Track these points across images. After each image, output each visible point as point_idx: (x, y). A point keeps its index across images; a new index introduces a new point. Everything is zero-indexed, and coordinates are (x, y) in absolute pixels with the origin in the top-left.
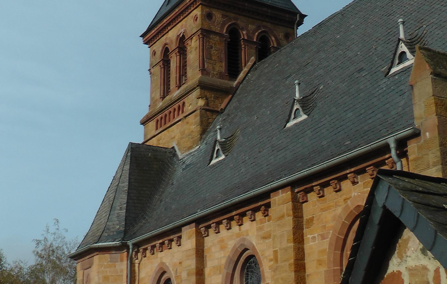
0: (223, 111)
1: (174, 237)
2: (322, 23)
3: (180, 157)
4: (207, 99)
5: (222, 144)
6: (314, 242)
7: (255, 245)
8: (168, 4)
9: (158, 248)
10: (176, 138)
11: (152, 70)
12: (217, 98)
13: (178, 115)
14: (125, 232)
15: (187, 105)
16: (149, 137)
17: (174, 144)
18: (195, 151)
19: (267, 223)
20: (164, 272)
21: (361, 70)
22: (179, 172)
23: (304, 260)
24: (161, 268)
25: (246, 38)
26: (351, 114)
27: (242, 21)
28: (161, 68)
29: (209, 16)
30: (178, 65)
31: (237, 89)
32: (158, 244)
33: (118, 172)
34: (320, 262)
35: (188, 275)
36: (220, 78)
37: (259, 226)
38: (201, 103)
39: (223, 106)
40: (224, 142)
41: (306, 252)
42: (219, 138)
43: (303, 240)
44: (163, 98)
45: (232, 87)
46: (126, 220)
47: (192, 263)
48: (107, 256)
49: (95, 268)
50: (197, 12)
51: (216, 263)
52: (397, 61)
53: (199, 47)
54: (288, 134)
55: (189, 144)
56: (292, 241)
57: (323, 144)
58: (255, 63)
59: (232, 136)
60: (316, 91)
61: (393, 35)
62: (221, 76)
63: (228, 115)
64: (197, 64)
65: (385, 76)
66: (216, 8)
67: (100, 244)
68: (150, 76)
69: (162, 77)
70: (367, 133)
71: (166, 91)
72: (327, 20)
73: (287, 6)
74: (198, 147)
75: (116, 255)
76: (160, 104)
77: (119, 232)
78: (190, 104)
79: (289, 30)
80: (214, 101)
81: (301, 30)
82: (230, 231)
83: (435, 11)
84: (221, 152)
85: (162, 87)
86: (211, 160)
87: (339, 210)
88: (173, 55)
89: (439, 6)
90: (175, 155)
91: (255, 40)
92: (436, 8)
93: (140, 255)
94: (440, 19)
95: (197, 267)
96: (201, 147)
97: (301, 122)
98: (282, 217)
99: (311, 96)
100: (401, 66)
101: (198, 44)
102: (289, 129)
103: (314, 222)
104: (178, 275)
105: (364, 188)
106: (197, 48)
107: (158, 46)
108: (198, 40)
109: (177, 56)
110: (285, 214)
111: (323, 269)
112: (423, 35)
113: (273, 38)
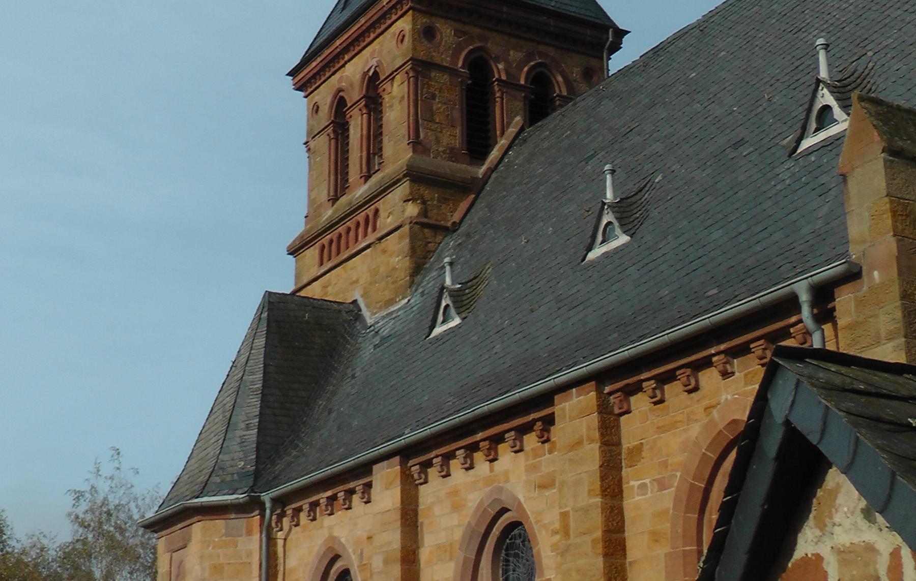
0: (456, 226)
1: (357, 484)
2: (660, 47)
3: (369, 321)
4: (424, 202)
5: (454, 295)
7: (522, 501)
8: (343, 9)
9: (324, 508)
10: (361, 282)
11: (312, 144)
12: (444, 200)
13: (365, 234)
14: (257, 475)
15: (382, 214)
16: (305, 280)
17: (357, 296)
18: (399, 309)
19: (547, 456)
20: (336, 557)
22: (367, 351)
23: (624, 531)
24: (330, 549)
25: (504, 77)
27: (494, 44)
28: (330, 140)
29: (428, 33)
30: (365, 132)
31: (486, 182)
32: (325, 500)
33: (242, 351)
34: (655, 537)
35: (386, 562)
36: (450, 159)
38: (412, 210)
39: (456, 217)
40: (459, 290)
41: (628, 514)
42: (448, 281)
43: (621, 491)
44: (334, 200)
45: (474, 179)
46: (258, 449)
47: (393, 539)
48: (219, 524)
49: (194, 547)
50: (404, 25)
51: (442, 537)
52: (813, 125)
55: (387, 295)
56: (598, 492)
57: (661, 294)
58: (522, 130)
60: (648, 185)
61: (805, 72)
62: (453, 154)
63: (468, 235)
64: (403, 130)
65: (790, 156)
67: (205, 499)
69: (333, 158)
70: (752, 272)
71: (340, 186)
72: (669, 40)
73: (588, 13)
74: (406, 300)
75: (239, 522)
76: (328, 213)
77: (243, 475)
78: (390, 213)
79: (593, 62)
80: (439, 208)
81: (617, 62)
82: (471, 472)
83: (892, 24)
84: (452, 311)
85: (332, 177)
86: (432, 327)
87: (695, 430)
88: (355, 112)
90: (358, 317)
91: (522, 82)
92: (893, 16)
93: (286, 521)
95: (403, 547)
96: (412, 301)
97: (617, 250)
98: (579, 443)
99: (638, 197)
100: (822, 135)
101: (406, 90)
103: (644, 454)
104: (364, 562)
105: (746, 384)
106: (403, 98)
107: (324, 95)
109: (362, 115)
111: (662, 550)
112: (866, 72)
113: (560, 79)
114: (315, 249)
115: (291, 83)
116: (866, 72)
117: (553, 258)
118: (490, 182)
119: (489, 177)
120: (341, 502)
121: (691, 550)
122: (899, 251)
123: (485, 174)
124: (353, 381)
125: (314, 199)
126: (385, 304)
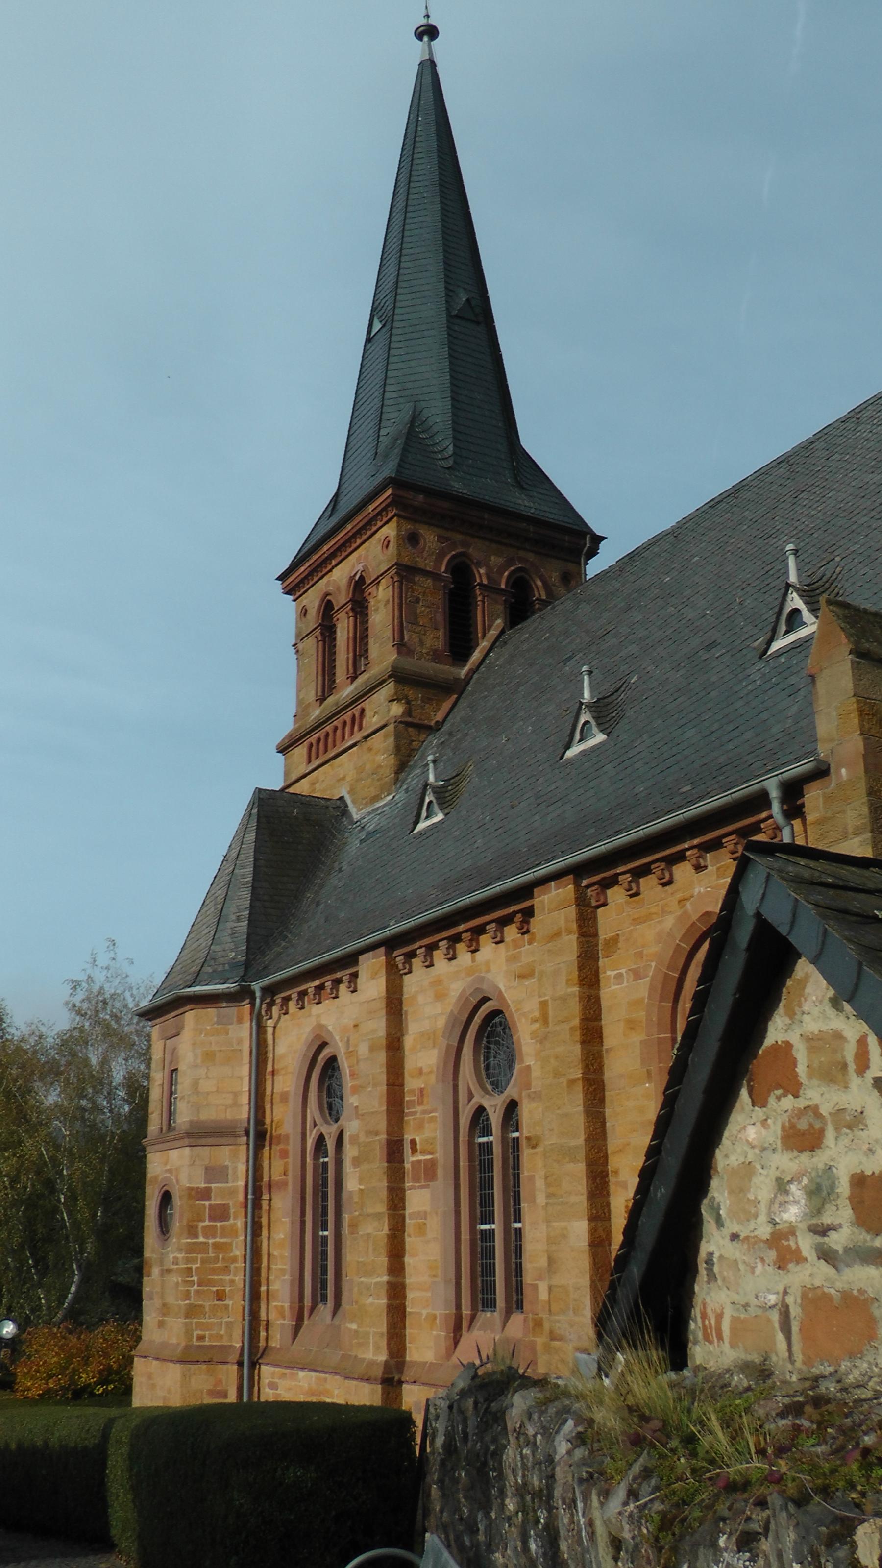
0: (439, 725)
3: (356, 816)
4: (408, 702)
5: (438, 791)
6: (619, 984)
7: (503, 990)
8: (331, 516)
9: (312, 997)
10: (348, 779)
11: (300, 646)
12: (427, 700)
13: (352, 733)
14: (247, 965)
16: (294, 777)
17: (344, 792)
19: (527, 947)
20: (324, 1045)
21: (712, 645)
22: (353, 846)
25: (485, 582)
27: (476, 550)
28: (318, 642)
29: (412, 539)
30: (351, 635)
31: (468, 683)
32: (313, 989)
33: (233, 846)
35: (372, 1049)
36: (433, 661)
37: (510, 953)
38: (397, 709)
39: (439, 717)
40: (442, 786)
41: (605, 1003)
42: (431, 778)
44: (322, 700)
45: (457, 680)
46: (248, 941)
47: (378, 1026)
48: (211, 1012)
49: (187, 1035)
50: (389, 531)
52: (783, 628)
53: (393, 601)
54: (568, 771)
55: (373, 792)
57: (637, 790)
58: (502, 632)
60: (625, 686)
62: (436, 656)
63: (451, 734)
64: (389, 633)
65: (760, 657)
69: (320, 659)
70: (724, 769)
71: (328, 686)
74: (391, 797)
75: (230, 1011)
76: (316, 713)
77: (234, 965)
79: (571, 567)
80: (422, 707)
81: (594, 567)
84: (436, 807)
85: (320, 678)
86: (416, 823)
87: (669, 922)
88: (342, 615)
90: (345, 812)
91: (503, 586)
92: (860, 522)
93: (275, 1010)
97: (594, 748)
98: (558, 934)
99: (614, 697)
100: (792, 638)
101: (391, 593)
102: (571, 761)
103: (620, 945)
104: (351, 1049)
105: (719, 877)
106: (388, 601)
107: (312, 598)
111: (637, 1038)
112: (834, 576)
113: (539, 583)
114: (386, 736)
115: (281, 587)
122: (865, 749)
123: (467, 675)
124: (340, 875)
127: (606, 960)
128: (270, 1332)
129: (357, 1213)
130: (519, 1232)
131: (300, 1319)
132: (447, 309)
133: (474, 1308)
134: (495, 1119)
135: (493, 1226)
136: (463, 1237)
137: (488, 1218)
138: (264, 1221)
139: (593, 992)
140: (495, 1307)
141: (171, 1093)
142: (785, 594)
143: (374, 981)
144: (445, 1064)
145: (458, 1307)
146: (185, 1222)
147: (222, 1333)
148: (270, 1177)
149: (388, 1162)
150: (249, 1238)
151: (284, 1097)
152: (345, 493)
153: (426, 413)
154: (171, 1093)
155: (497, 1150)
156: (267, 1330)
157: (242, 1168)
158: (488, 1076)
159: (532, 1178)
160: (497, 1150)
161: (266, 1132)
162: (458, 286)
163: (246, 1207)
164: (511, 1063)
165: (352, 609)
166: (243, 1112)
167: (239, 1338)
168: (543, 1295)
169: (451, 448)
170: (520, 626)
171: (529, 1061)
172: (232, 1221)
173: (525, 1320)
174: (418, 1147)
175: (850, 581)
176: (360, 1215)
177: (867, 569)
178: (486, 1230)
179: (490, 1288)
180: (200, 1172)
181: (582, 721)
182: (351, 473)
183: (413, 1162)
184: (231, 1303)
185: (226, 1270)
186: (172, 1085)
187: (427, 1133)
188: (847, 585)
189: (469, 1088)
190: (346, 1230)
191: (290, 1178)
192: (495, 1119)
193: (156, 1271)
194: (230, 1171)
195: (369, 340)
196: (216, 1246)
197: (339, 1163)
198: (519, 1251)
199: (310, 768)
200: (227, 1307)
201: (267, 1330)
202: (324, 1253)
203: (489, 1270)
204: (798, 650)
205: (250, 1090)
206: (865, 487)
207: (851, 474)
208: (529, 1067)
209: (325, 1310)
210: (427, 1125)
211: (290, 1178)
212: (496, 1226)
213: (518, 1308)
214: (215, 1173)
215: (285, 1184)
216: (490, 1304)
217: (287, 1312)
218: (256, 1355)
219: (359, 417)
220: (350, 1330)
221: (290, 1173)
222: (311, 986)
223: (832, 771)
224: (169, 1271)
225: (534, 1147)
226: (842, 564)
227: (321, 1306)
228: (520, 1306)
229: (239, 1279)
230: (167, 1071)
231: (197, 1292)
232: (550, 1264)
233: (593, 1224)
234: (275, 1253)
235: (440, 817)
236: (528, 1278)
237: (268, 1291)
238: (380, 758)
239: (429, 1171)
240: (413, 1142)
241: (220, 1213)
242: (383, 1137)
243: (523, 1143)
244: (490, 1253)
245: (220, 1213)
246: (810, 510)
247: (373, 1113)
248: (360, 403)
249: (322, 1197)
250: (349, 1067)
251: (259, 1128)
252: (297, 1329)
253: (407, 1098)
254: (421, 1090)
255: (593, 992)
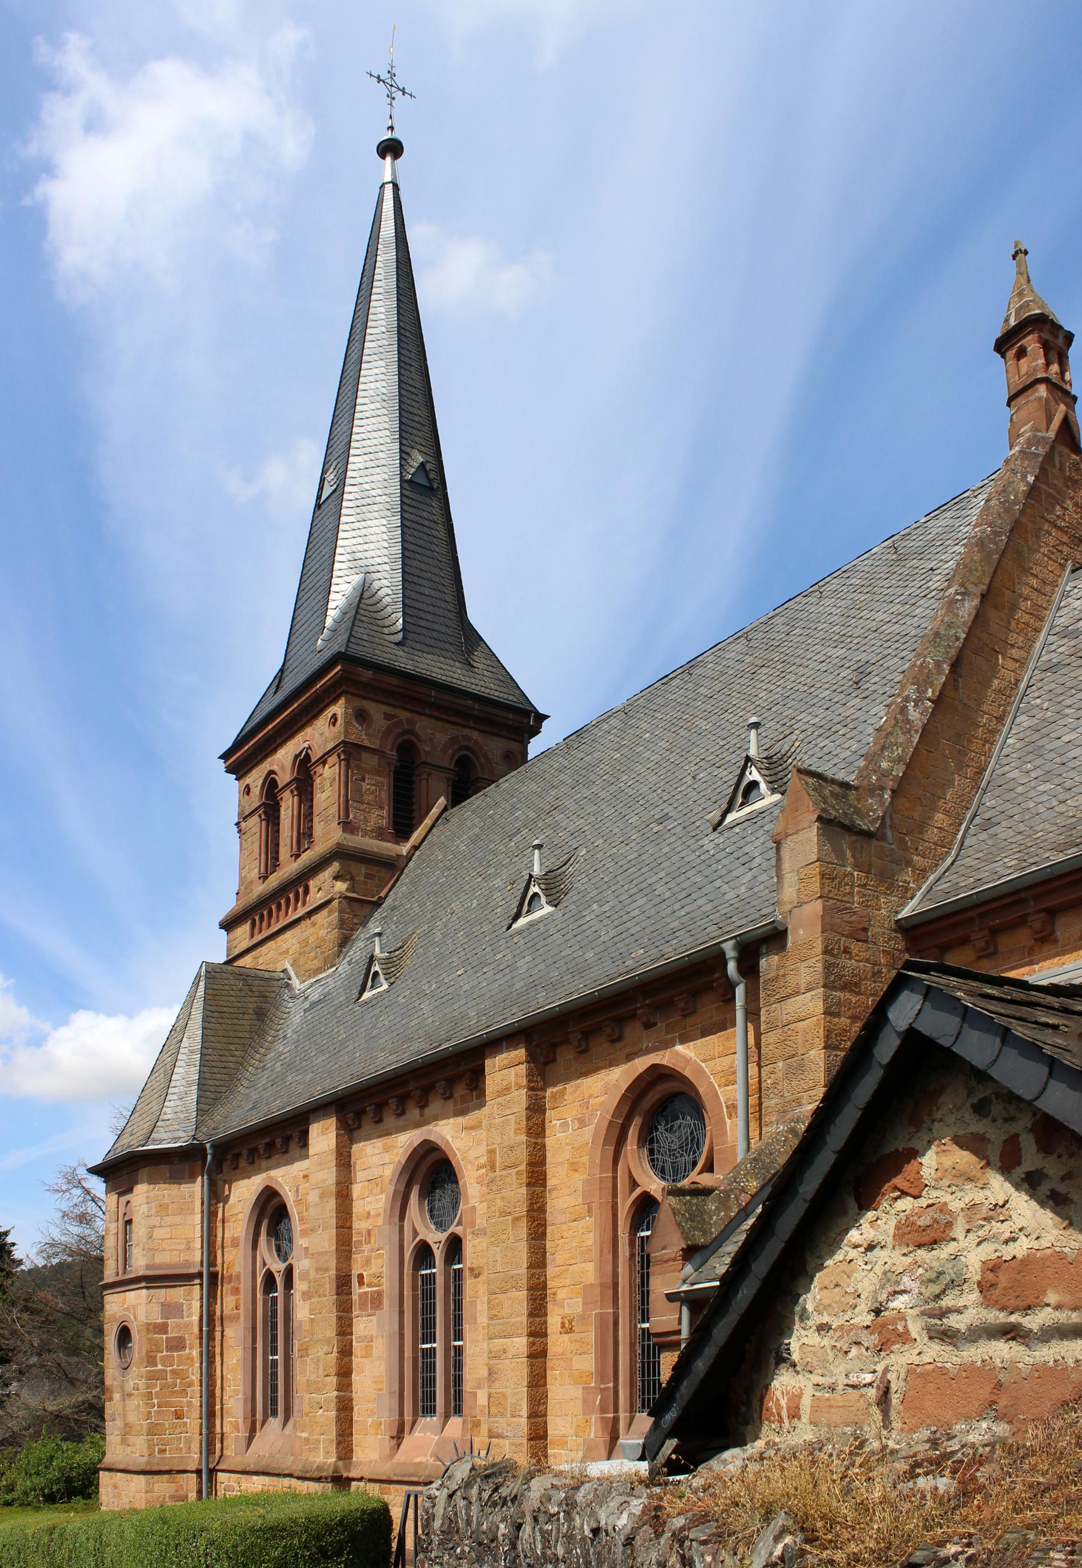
2: (584, 729)
6: (564, 1132)
7: (450, 1140)
8: (276, 692)
9: (262, 1152)
11: (243, 825)
13: (295, 909)
16: (236, 952)
18: (327, 977)
19: (475, 1101)
21: (666, 817)
23: (545, 1164)
26: (644, 900)
28: (261, 821)
29: (361, 716)
30: (295, 813)
31: (410, 860)
32: (263, 1145)
33: (181, 1016)
34: (574, 1167)
35: (322, 1196)
36: (377, 838)
37: (459, 1107)
42: (377, 951)
43: (544, 1129)
44: (264, 878)
45: (399, 856)
50: (338, 709)
51: (374, 1173)
52: (740, 800)
53: (340, 779)
54: (515, 940)
55: (316, 964)
56: (524, 1130)
57: (587, 956)
58: (445, 810)
59: (401, 948)
60: (572, 859)
61: (731, 750)
62: (380, 834)
63: (394, 908)
64: (334, 810)
65: (715, 829)
66: (373, 700)
68: (238, 835)
69: (263, 837)
70: (677, 934)
71: (272, 861)
72: (593, 723)
73: (511, 698)
74: (334, 969)
76: (260, 889)
78: (320, 889)
80: (366, 884)
81: (535, 747)
82: (403, 1118)
83: (820, 703)
84: (382, 977)
85: (263, 856)
86: (361, 993)
88: (287, 795)
89: (828, 692)
92: (822, 696)
94: (828, 718)
96: (339, 969)
97: (541, 920)
98: (507, 1089)
99: (563, 869)
100: (747, 810)
101: (338, 771)
103: (566, 1097)
104: (299, 1198)
105: (667, 1033)
106: (334, 779)
107: (256, 778)
108: (337, 765)
109: (293, 796)
110: (513, 1084)
111: (579, 1178)
112: (793, 749)
114: (330, 913)
115: (224, 765)
116: (793, 749)
117: (479, 927)
118: (414, 858)
119: (413, 854)
120: (279, 1146)
121: (607, 1177)
122: (824, 910)
123: (409, 853)
124: (286, 1041)
125: (245, 877)
126: (314, 972)
127: (553, 1111)
128: (225, 1443)
129: (307, 1339)
130: (459, 1351)
131: (253, 1431)
132: (401, 473)
133: (415, 1415)
134: (438, 1254)
135: (434, 1345)
136: (406, 1355)
137: (430, 1337)
138: (218, 1350)
139: (539, 1140)
140: (435, 1412)
141: (126, 1242)
142: (744, 768)
143: (325, 1137)
144: (392, 1207)
145: (401, 1413)
146: (144, 1354)
147: (181, 1446)
148: (222, 1311)
149: (337, 1294)
150: (204, 1365)
151: (235, 1243)
152: (291, 669)
153: (376, 585)
154: (126, 1242)
155: (440, 1281)
156: (222, 1442)
157: (196, 1304)
158: (432, 1217)
159: (474, 1304)
160: (440, 1281)
161: (218, 1273)
162: (413, 448)
163: (201, 1338)
164: (455, 1204)
165: (296, 788)
166: (196, 1257)
167: (197, 1450)
168: (482, 1399)
169: (401, 621)
170: (463, 804)
171: (473, 1202)
172: (187, 1351)
173: (464, 1422)
174: (365, 1280)
175: (809, 753)
176: (310, 1340)
177: (827, 742)
178: (427, 1349)
179: (430, 1397)
180: (157, 1309)
181: (530, 893)
182: (298, 647)
183: (360, 1295)
184: (188, 1420)
185: (184, 1392)
186: (126, 1234)
187: (374, 1269)
188: (806, 757)
189: (414, 1227)
190: (296, 1353)
191: (241, 1311)
192: (438, 1254)
193: (117, 1396)
194: (185, 1308)
195: (318, 506)
196: (173, 1372)
197: (288, 1297)
198: (459, 1365)
199: (258, 938)
200: (185, 1424)
201: (222, 1442)
202: (274, 1375)
203: (430, 1382)
204: (754, 821)
205: (202, 1236)
206: (827, 661)
207: (814, 649)
208: (474, 1208)
209: (274, 1423)
210: (373, 1261)
211: (241, 1311)
212: (438, 1345)
213: (455, 1412)
214: (171, 1310)
215: (237, 1317)
216: (430, 1410)
217: (241, 1426)
218: (213, 1462)
219: (306, 590)
220: (301, 1438)
221: (242, 1307)
222: (261, 1144)
223: (789, 932)
224: (130, 1395)
225: (477, 1276)
226: (801, 737)
227: (271, 1419)
228: (458, 1410)
229: (196, 1402)
230: (121, 1222)
231: (157, 1412)
232: (490, 1375)
233: (531, 1339)
234: (228, 1376)
235: (385, 986)
236: (467, 1387)
237: (222, 1408)
238: (323, 932)
239: (376, 1301)
240: (361, 1277)
241: (177, 1344)
242: (333, 1273)
243: (466, 1274)
244: (431, 1367)
245: (177, 1344)
246: (769, 685)
247: (323, 1253)
248: (308, 575)
249: (272, 1326)
250: (298, 1213)
251: (212, 1269)
252: (250, 1439)
253: (354, 1239)
254: (369, 1232)
255: (539, 1140)
